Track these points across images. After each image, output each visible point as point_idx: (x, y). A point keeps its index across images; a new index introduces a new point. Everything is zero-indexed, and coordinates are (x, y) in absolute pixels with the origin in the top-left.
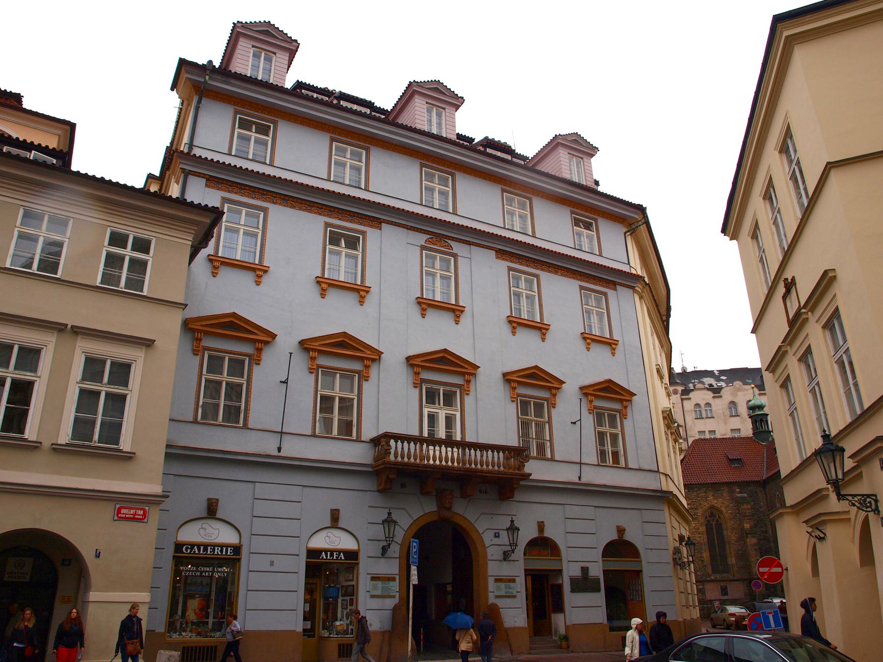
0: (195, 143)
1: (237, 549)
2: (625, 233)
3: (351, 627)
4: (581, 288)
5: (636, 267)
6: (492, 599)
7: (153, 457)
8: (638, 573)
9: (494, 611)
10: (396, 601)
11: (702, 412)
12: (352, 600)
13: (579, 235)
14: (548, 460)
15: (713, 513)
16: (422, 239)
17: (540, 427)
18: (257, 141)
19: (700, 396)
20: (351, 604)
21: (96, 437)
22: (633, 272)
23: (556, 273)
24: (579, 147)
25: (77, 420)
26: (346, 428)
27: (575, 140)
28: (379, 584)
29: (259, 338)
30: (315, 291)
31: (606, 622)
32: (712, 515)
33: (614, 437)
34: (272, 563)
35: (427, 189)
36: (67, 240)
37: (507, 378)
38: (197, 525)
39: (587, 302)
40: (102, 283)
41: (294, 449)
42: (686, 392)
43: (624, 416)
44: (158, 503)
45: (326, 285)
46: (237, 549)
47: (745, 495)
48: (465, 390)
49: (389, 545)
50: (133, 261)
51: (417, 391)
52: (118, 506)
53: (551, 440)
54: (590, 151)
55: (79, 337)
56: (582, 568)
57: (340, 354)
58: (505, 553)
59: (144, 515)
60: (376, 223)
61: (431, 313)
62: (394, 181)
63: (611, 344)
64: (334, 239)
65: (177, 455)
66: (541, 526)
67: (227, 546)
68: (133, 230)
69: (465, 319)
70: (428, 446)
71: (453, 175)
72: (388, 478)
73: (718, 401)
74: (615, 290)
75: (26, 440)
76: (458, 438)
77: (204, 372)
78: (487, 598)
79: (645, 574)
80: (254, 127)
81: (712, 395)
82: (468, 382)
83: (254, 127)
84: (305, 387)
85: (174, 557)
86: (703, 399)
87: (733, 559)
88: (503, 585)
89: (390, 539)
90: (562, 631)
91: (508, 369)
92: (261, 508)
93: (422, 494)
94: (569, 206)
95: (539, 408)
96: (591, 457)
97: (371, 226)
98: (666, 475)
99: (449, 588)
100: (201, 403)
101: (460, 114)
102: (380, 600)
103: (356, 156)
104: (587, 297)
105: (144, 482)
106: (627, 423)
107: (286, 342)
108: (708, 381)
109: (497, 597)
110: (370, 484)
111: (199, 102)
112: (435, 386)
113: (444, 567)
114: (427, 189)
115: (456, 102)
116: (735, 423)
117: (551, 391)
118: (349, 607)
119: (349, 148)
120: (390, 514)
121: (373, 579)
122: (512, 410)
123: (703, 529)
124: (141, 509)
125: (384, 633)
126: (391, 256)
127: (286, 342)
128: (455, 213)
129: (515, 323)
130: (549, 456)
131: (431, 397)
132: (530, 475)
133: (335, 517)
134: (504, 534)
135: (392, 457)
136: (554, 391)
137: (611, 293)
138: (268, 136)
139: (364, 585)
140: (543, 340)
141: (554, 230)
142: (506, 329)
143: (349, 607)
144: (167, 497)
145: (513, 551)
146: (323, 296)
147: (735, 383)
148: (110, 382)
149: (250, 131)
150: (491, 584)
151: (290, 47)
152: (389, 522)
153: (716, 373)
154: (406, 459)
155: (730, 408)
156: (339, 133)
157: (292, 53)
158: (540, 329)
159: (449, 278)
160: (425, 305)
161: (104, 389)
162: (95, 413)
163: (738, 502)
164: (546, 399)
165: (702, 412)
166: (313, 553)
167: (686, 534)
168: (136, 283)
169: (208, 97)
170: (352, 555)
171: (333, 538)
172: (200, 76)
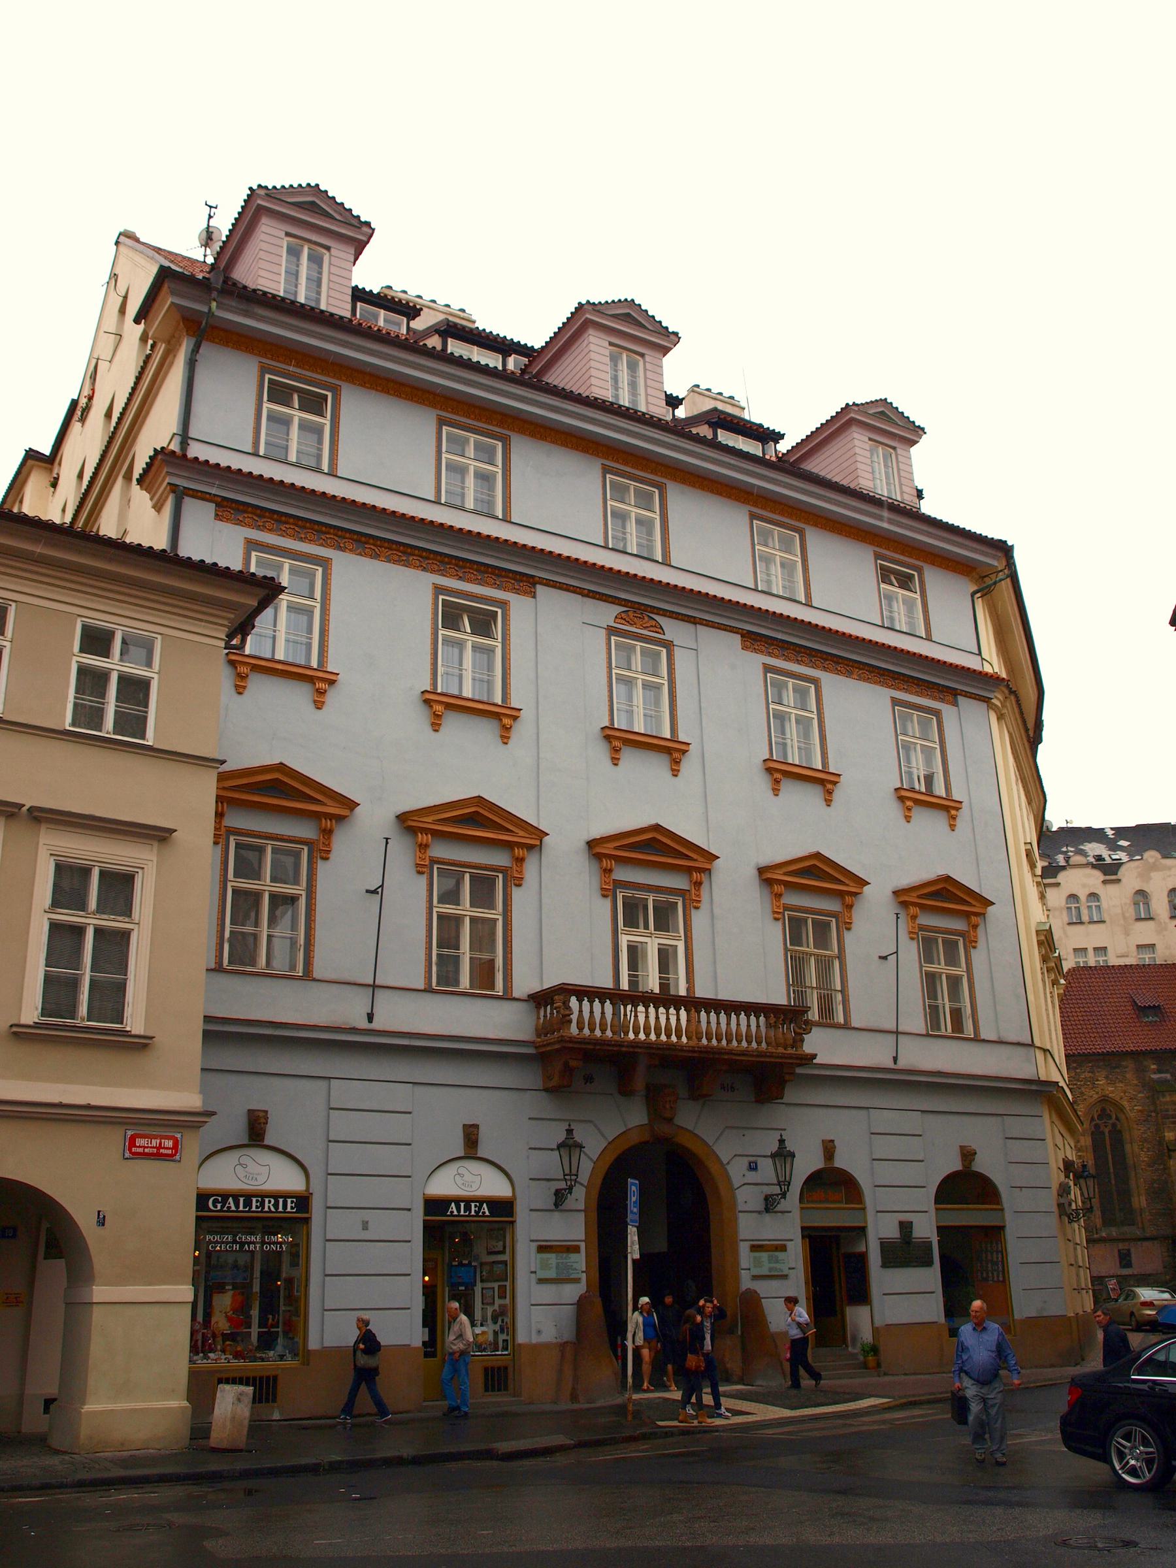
1: (303, 1201)
2: (973, 595)
3: (502, 1337)
4: (895, 702)
5: (993, 664)
6: (746, 1283)
7: (183, 1044)
8: (995, 1232)
9: (751, 1304)
10: (580, 1289)
11: (1080, 911)
12: (503, 1289)
13: (890, 598)
14: (838, 1026)
15: (1106, 1109)
16: (608, 614)
17: (825, 966)
18: (303, 426)
19: (1078, 880)
20: (502, 1296)
21: (83, 1009)
22: (988, 669)
23: (849, 674)
24: (890, 426)
25: (48, 980)
26: (484, 974)
27: (882, 413)
28: (552, 1258)
29: (325, 810)
30: (419, 718)
31: (942, 1320)
32: (1103, 1114)
33: (954, 982)
34: (365, 1226)
35: (615, 514)
36: (8, 644)
37: (767, 876)
38: (231, 1158)
39: (904, 727)
40: (73, 724)
42: (1051, 871)
43: (971, 943)
44: (196, 1126)
45: (440, 706)
46: (303, 1201)
47: (1168, 1076)
48: (692, 901)
49: (570, 1188)
50: (124, 679)
51: (608, 903)
52: (129, 1133)
53: (844, 991)
55: (43, 827)
56: (901, 1224)
57: (476, 842)
58: (767, 1198)
60: (526, 584)
61: (629, 757)
62: (557, 503)
63: (949, 808)
64: (451, 617)
65: (220, 1033)
66: (829, 1149)
67: (285, 1196)
68: (120, 621)
69: (689, 765)
71: (662, 488)
72: (566, 1064)
73: (1111, 888)
74: (955, 704)
75: (126, 1034)
76: (682, 992)
77: (231, 875)
79: (1011, 1234)
80: (296, 397)
81: (1102, 877)
82: (698, 884)
83: (296, 397)
84: (410, 899)
85: (198, 1218)
86: (1084, 886)
87: (1143, 1199)
88: (764, 1256)
89: (571, 1177)
90: (867, 1336)
91: (765, 861)
92: (342, 1125)
93: (620, 1093)
94: (871, 543)
95: (822, 929)
96: (915, 1021)
97: (517, 591)
98: (1045, 1051)
100: (227, 935)
101: (670, 361)
103: (644, 501)
104: (905, 719)
105: (167, 1087)
106: (978, 956)
107: (374, 818)
108: (1094, 849)
109: (756, 1278)
110: (530, 1077)
111: (196, 350)
112: (639, 895)
113: (659, 1222)
114: (615, 514)
115: (663, 339)
116: (1145, 933)
117: (690, 875)
118: (498, 1302)
119: (473, 437)
120: (570, 1131)
121: (542, 1249)
122: (775, 935)
124: (168, 1138)
125: (563, 1345)
126: (556, 650)
127: (374, 818)
128: (666, 563)
129: (779, 773)
130: (841, 1019)
131: (632, 914)
132: (814, 1056)
133: (471, 1137)
134: (766, 1165)
135: (574, 1030)
136: (848, 899)
137: (947, 710)
138: (322, 415)
139: (526, 1260)
140: (828, 802)
141: (842, 590)
142: (763, 783)
143: (498, 1302)
144: (213, 1114)
145: (784, 1195)
146: (436, 727)
147: (1147, 855)
148: (101, 909)
149: (288, 404)
150: (745, 1257)
151: (355, 234)
152: (569, 1146)
153: (1110, 833)
154: (598, 1033)
155: (1136, 904)
156: (453, 409)
158: (822, 782)
159: (658, 687)
160: (618, 741)
161: (91, 921)
162: (77, 965)
163: (1154, 1090)
164: (503, 870)
165: (1080, 911)
166: (435, 1205)
167: (1071, 1155)
168: (132, 723)
169: (212, 340)
170: (503, 1208)
171: (468, 1177)
172: (201, 302)
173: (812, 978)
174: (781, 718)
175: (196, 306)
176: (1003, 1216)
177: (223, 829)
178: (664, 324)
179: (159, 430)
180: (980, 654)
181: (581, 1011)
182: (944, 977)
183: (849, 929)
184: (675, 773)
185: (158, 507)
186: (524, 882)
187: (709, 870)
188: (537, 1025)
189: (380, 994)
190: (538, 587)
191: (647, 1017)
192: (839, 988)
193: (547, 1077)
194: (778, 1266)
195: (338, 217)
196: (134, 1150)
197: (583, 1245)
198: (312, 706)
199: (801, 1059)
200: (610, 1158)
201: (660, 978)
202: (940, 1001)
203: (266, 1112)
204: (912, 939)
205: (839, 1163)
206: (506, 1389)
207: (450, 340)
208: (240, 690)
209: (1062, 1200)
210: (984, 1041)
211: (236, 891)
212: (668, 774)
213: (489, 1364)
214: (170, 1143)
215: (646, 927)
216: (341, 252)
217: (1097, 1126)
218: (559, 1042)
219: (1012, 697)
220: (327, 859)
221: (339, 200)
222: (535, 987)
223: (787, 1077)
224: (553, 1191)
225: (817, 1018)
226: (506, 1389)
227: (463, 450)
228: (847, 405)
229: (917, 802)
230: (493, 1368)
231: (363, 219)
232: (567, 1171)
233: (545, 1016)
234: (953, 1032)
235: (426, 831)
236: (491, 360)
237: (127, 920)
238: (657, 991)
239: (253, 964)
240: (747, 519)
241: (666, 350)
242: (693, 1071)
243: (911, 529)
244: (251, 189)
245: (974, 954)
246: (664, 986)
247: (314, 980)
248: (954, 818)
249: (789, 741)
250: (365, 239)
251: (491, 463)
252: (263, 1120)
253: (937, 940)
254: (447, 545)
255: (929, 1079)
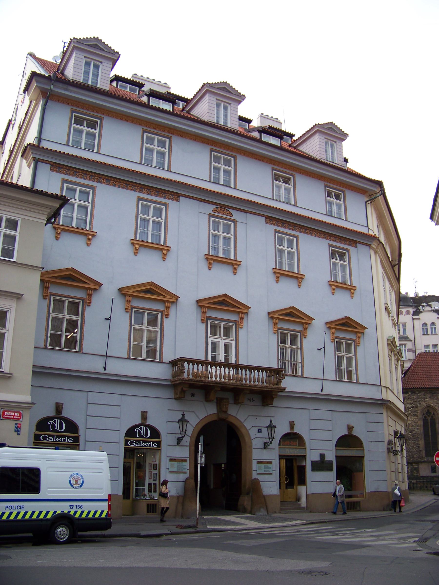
0: (43, 137)
2: (366, 202)
6: (254, 475)
7: (25, 376)
9: (256, 484)
10: (187, 475)
16: (210, 208)
17: (294, 353)
22: (371, 233)
23: (311, 234)
26: (151, 353)
27: (331, 128)
28: (175, 463)
32: (428, 412)
33: (349, 360)
37: (272, 316)
41: (116, 368)
43: (357, 344)
49: (183, 437)
51: (204, 325)
52: (3, 410)
54: (341, 136)
56: (320, 454)
58: (265, 443)
59: (20, 416)
60: (176, 196)
62: (190, 164)
64: (333, 254)
65: (40, 372)
66: (292, 425)
69: (240, 271)
70: (211, 367)
72: (182, 389)
74: (356, 247)
76: (234, 362)
78: (251, 474)
82: (242, 319)
88: (263, 465)
89: (183, 433)
92: (92, 410)
94: (323, 181)
96: (331, 374)
99: (223, 466)
102: (175, 475)
106: (359, 349)
109: (259, 474)
110: (169, 393)
111: (45, 104)
115: (239, 98)
117: (239, 314)
119: (157, 137)
120: (183, 415)
121: (171, 460)
122: (274, 340)
123: (421, 423)
124: (18, 412)
125: (178, 497)
127: (109, 290)
128: (235, 188)
131: (214, 330)
132: (285, 388)
134: (265, 430)
135: (185, 376)
136: (305, 326)
138: (95, 129)
141: (310, 200)
142: (272, 278)
144: (35, 404)
145: (271, 442)
149: (82, 125)
150: (255, 466)
152: (183, 420)
156: (148, 126)
157: (114, 62)
164: (235, 322)
169: (52, 100)
173: (289, 357)
174: (281, 252)
175: (49, 85)
176: (306, 451)
177: (49, 294)
178: (239, 92)
179: (31, 137)
180: (368, 227)
181: (189, 368)
182: (345, 358)
183: (305, 338)
184: (235, 273)
185: (29, 166)
186: (307, 336)
187: (247, 313)
188: (172, 373)
189: (109, 360)
190: (181, 197)
191: (220, 372)
192: (300, 361)
193: (176, 394)
194: (268, 470)
195: (106, 50)
196: (4, 416)
197: (188, 459)
198: (55, 239)
199: (281, 389)
200: (200, 426)
201: (225, 356)
202: (343, 367)
203: (63, 404)
204: (332, 342)
205: (295, 431)
206: (156, 512)
207: (151, 98)
208: (57, 239)
209: (389, 447)
210: (360, 383)
211: (53, 318)
212: (296, 286)
213: (150, 503)
214: (18, 414)
215: (220, 336)
216: (106, 64)
217: (425, 417)
218: (180, 380)
219: (381, 244)
220: (90, 306)
221: (106, 43)
222: (172, 358)
223: (274, 396)
224: (263, 443)
225: (290, 373)
226: (156, 512)
227: (153, 142)
228: (316, 124)
229: (337, 286)
230: (151, 504)
231: (116, 51)
232: (181, 431)
233: (175, 370)
234: (347, 379)
235: (129, 295)
236: (167, 107)
237: (4, 329)
238: (223, 361)
239: (60, 347)
240: (323, 187)
241: (240, 102)
242: (236, 393)
243: (189, 126)
244: (71, 39)
245: (358, 349)
246: (227, 359)
247: (83, 353)
248: (353, 293)
249: (338, 274)
250: (116, 59)
251: (164, 147)
252: (61, 407)
253: (343, 343)
254: (160, 185)
255: (363, 401)
